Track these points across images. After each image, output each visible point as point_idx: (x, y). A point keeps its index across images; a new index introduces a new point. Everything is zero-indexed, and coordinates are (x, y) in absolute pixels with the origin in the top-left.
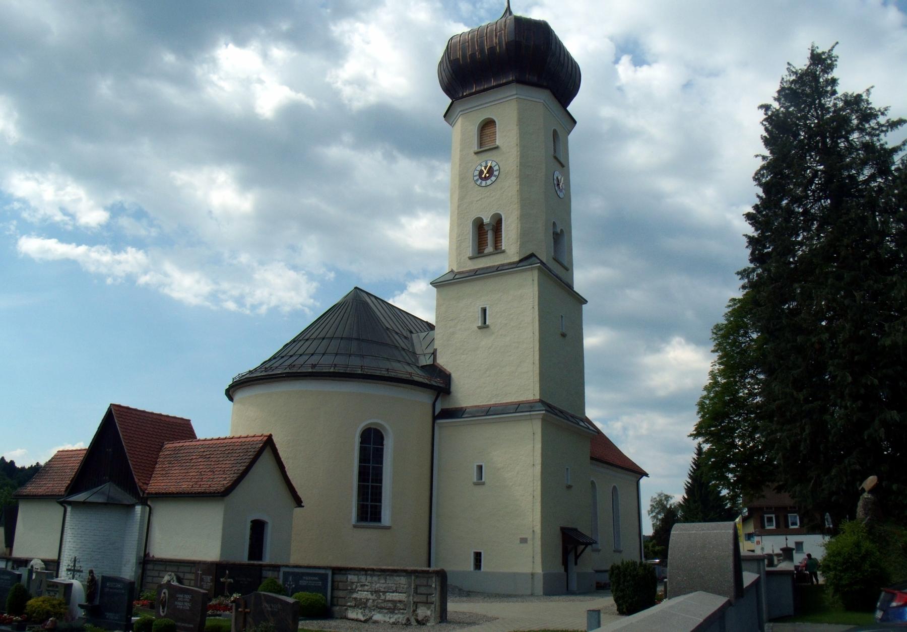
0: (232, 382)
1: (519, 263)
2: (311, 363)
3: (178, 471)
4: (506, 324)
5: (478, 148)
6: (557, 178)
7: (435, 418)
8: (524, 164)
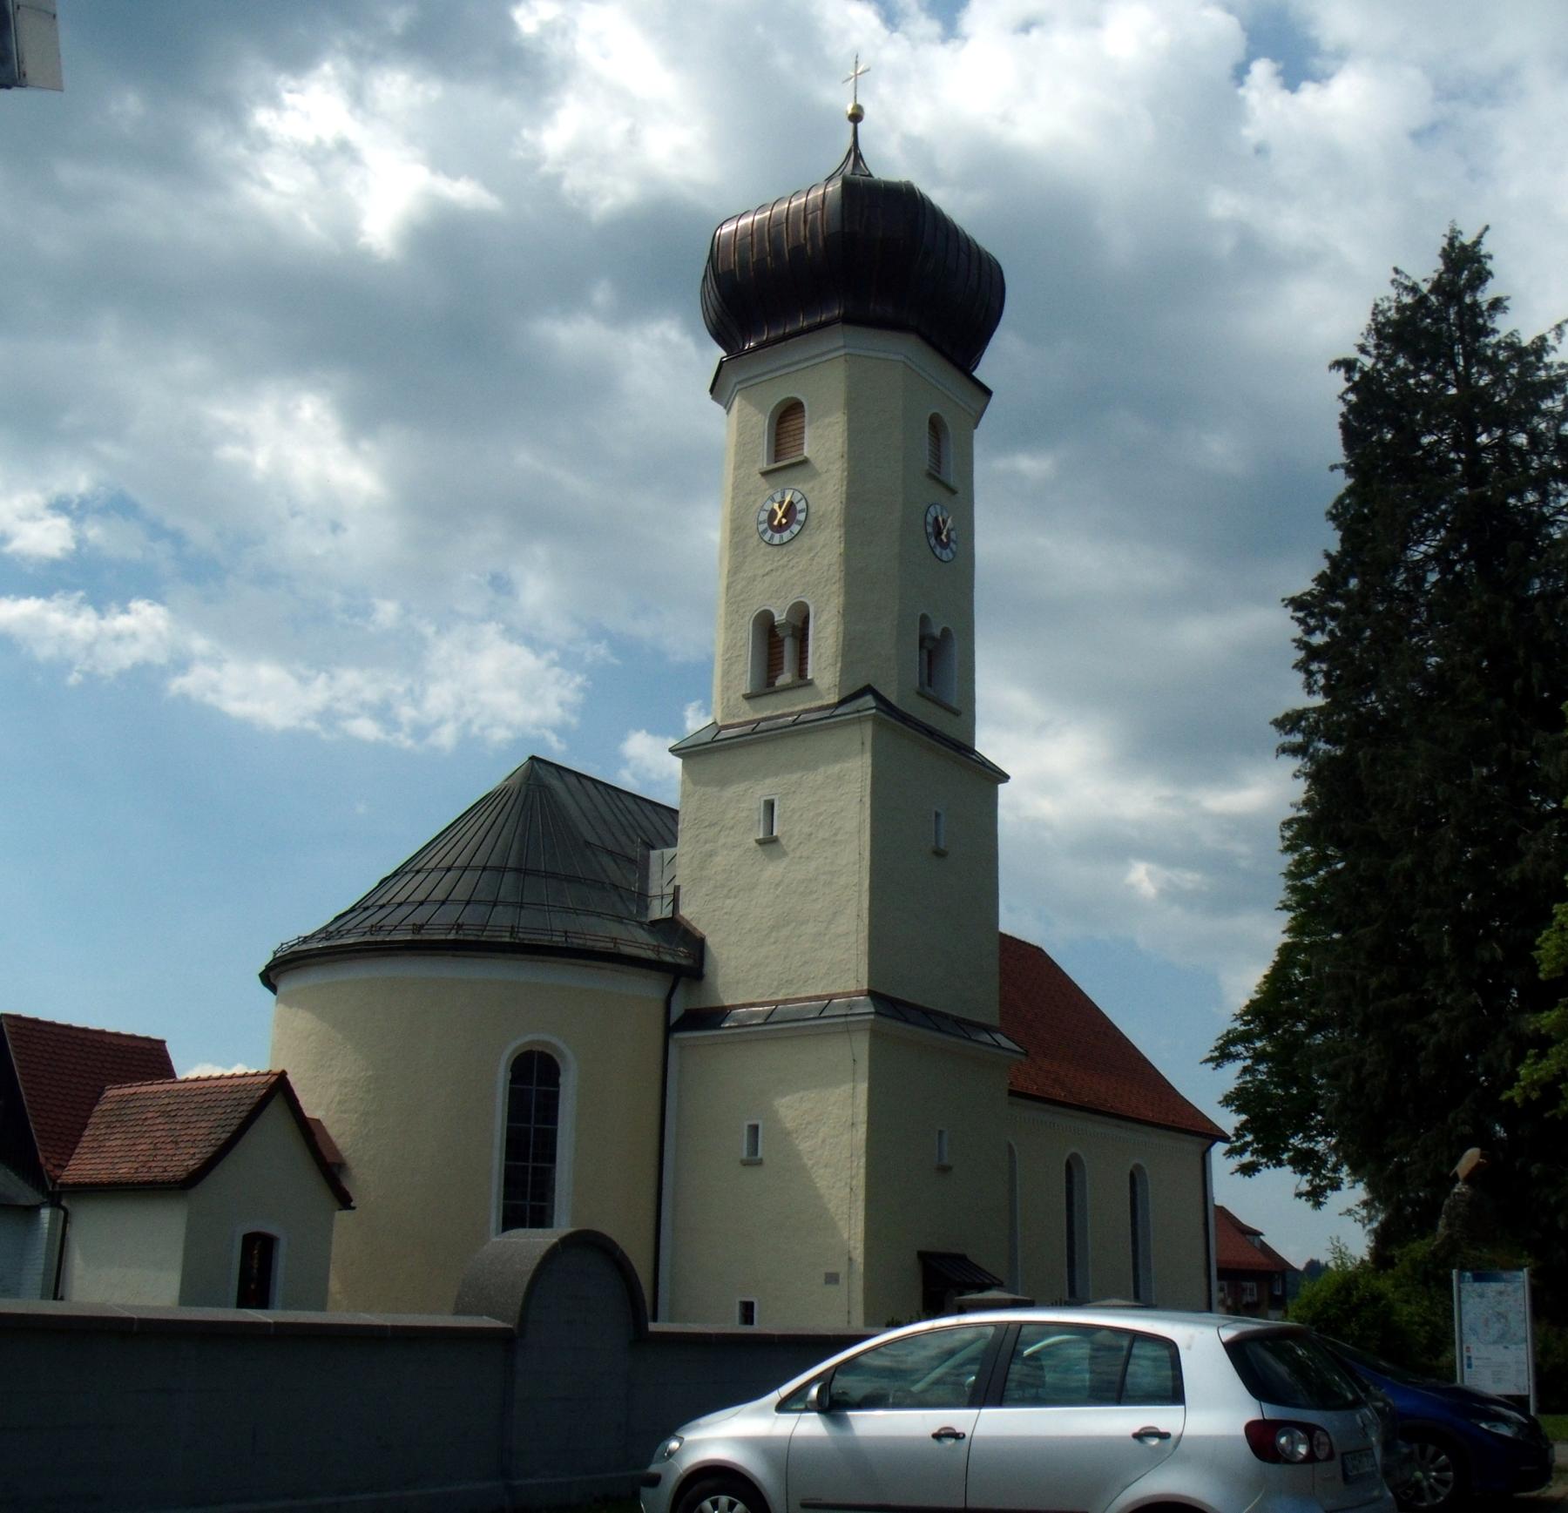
0: (271, 958)
1: (837, 708)
2: (412, 923)
3: (119, 1142)
4: (811, 834)
5: (768, 464)
6: (936, 519)
7: (670, 1029)
8: (855, 498)
